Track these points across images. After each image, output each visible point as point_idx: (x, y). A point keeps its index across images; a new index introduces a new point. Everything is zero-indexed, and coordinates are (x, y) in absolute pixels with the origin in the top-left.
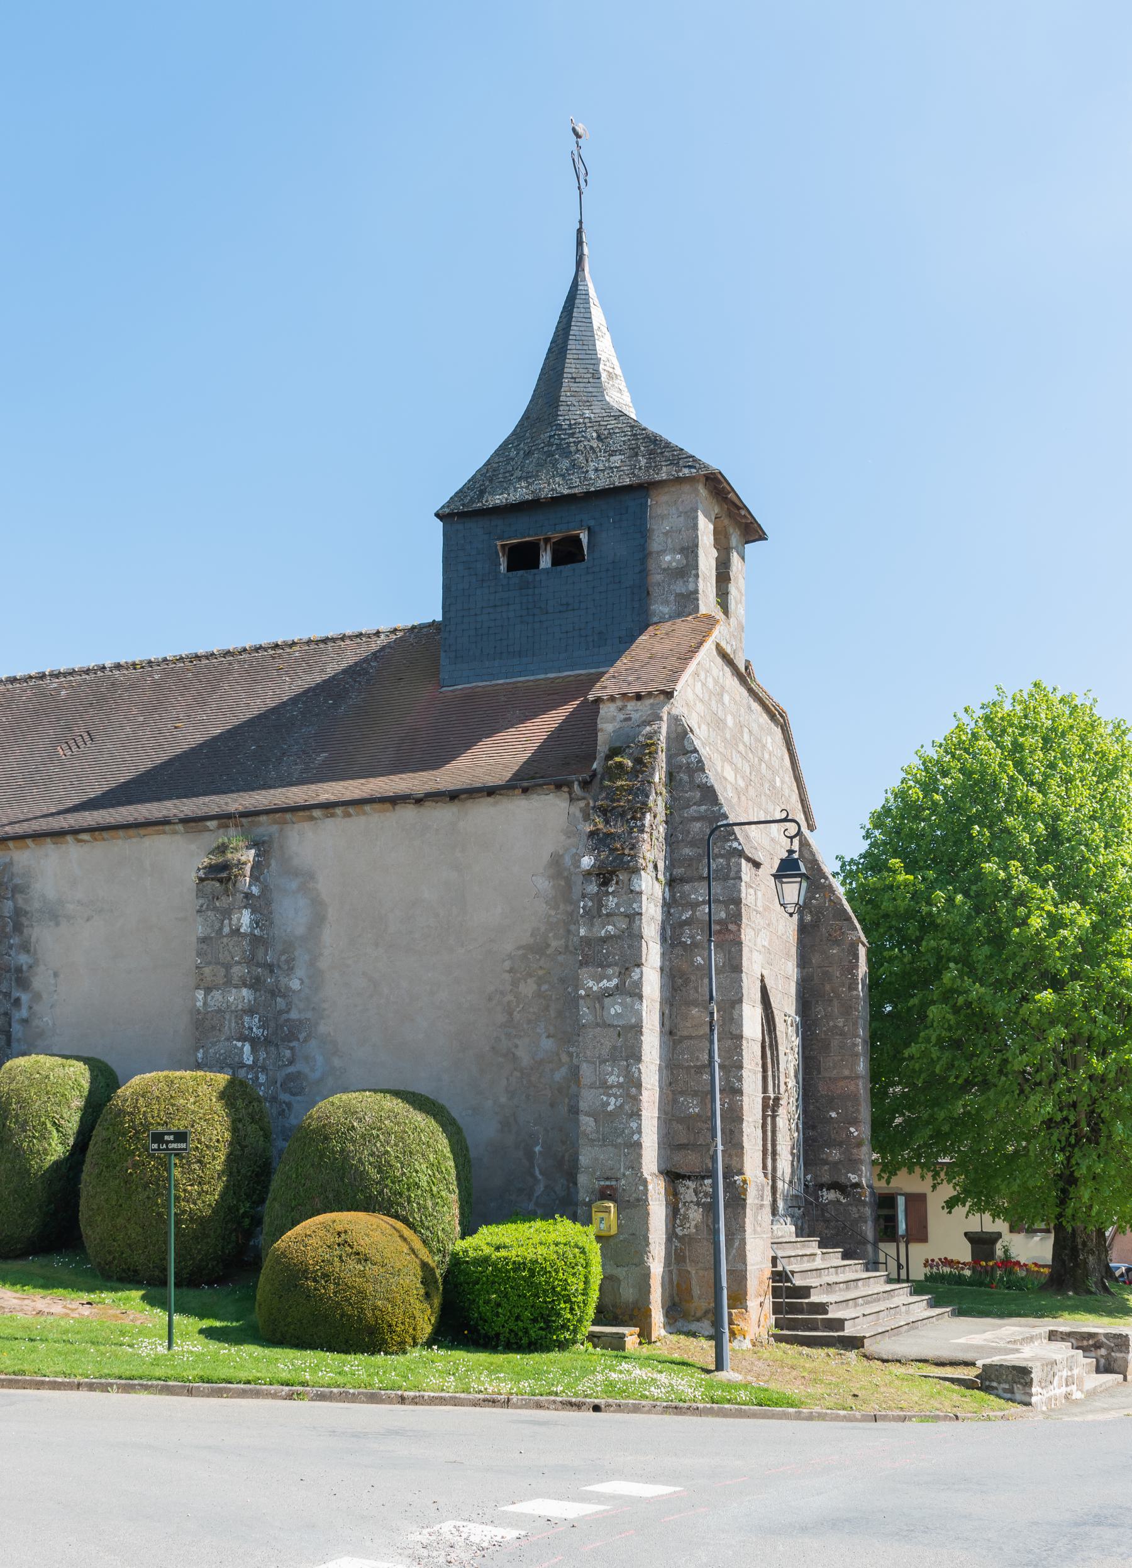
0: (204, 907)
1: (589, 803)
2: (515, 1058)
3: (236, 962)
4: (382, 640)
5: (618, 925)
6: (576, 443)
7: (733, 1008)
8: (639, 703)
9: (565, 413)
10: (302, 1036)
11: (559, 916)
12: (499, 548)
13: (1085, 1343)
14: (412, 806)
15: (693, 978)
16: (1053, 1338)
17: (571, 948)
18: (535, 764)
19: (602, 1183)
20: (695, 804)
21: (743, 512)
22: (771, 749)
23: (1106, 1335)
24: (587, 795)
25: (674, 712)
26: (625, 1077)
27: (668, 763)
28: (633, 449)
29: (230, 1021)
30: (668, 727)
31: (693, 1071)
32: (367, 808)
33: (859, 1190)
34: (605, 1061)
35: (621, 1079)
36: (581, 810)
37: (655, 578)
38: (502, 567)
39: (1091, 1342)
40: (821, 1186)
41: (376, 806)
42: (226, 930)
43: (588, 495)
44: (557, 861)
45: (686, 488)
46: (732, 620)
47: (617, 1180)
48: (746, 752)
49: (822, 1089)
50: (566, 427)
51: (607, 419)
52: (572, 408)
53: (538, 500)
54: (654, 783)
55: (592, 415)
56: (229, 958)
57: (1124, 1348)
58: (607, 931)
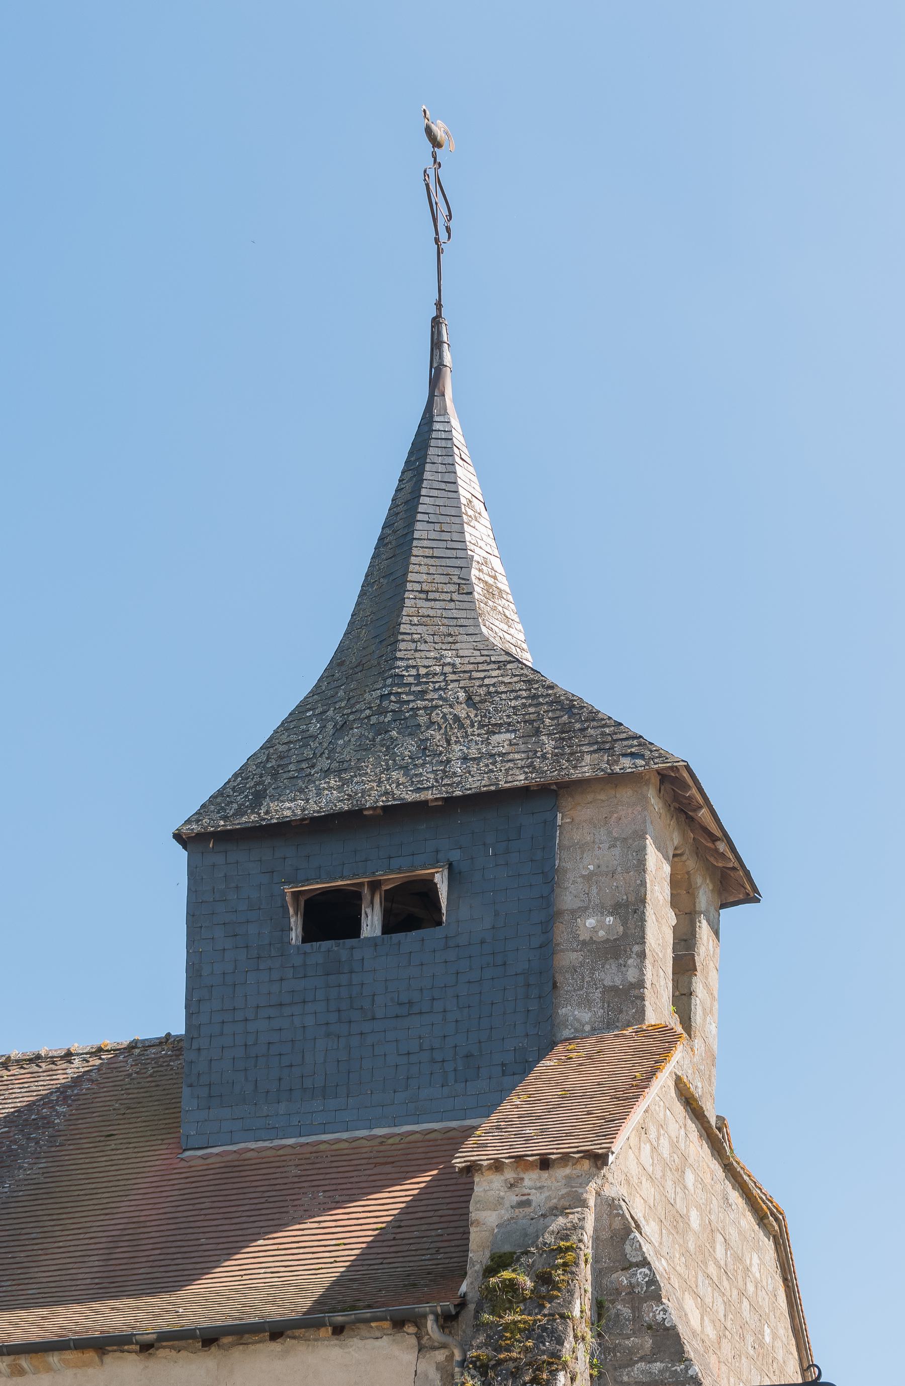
1: (453, 1355)
4: (77, 1067)
6: (429, 710)
8: (545, 1174)
9: (409, 655)
14: (133, 1356)
18: (355, 1286)
20: (642, 1359)
21: (722, 847)
22: (758, 1275)
24: (448, 1339)
25: (609, 1191)
27: (597, 1283)
28: (531, 722)
30: (597, 1220)
32: (54, 1359)
36: (439, 1367)
37: (569, 958)
38: (293, 935)
41: (69, 1355)
43: (451, 804)
45: (626, 794)
46: (698, 1043)
48: (720, 1278)
50: (411, 680)
51: (485, 667)
52: (422, 647)
53: (361, 811)
54: (572, 1319)
55: (458, 661)
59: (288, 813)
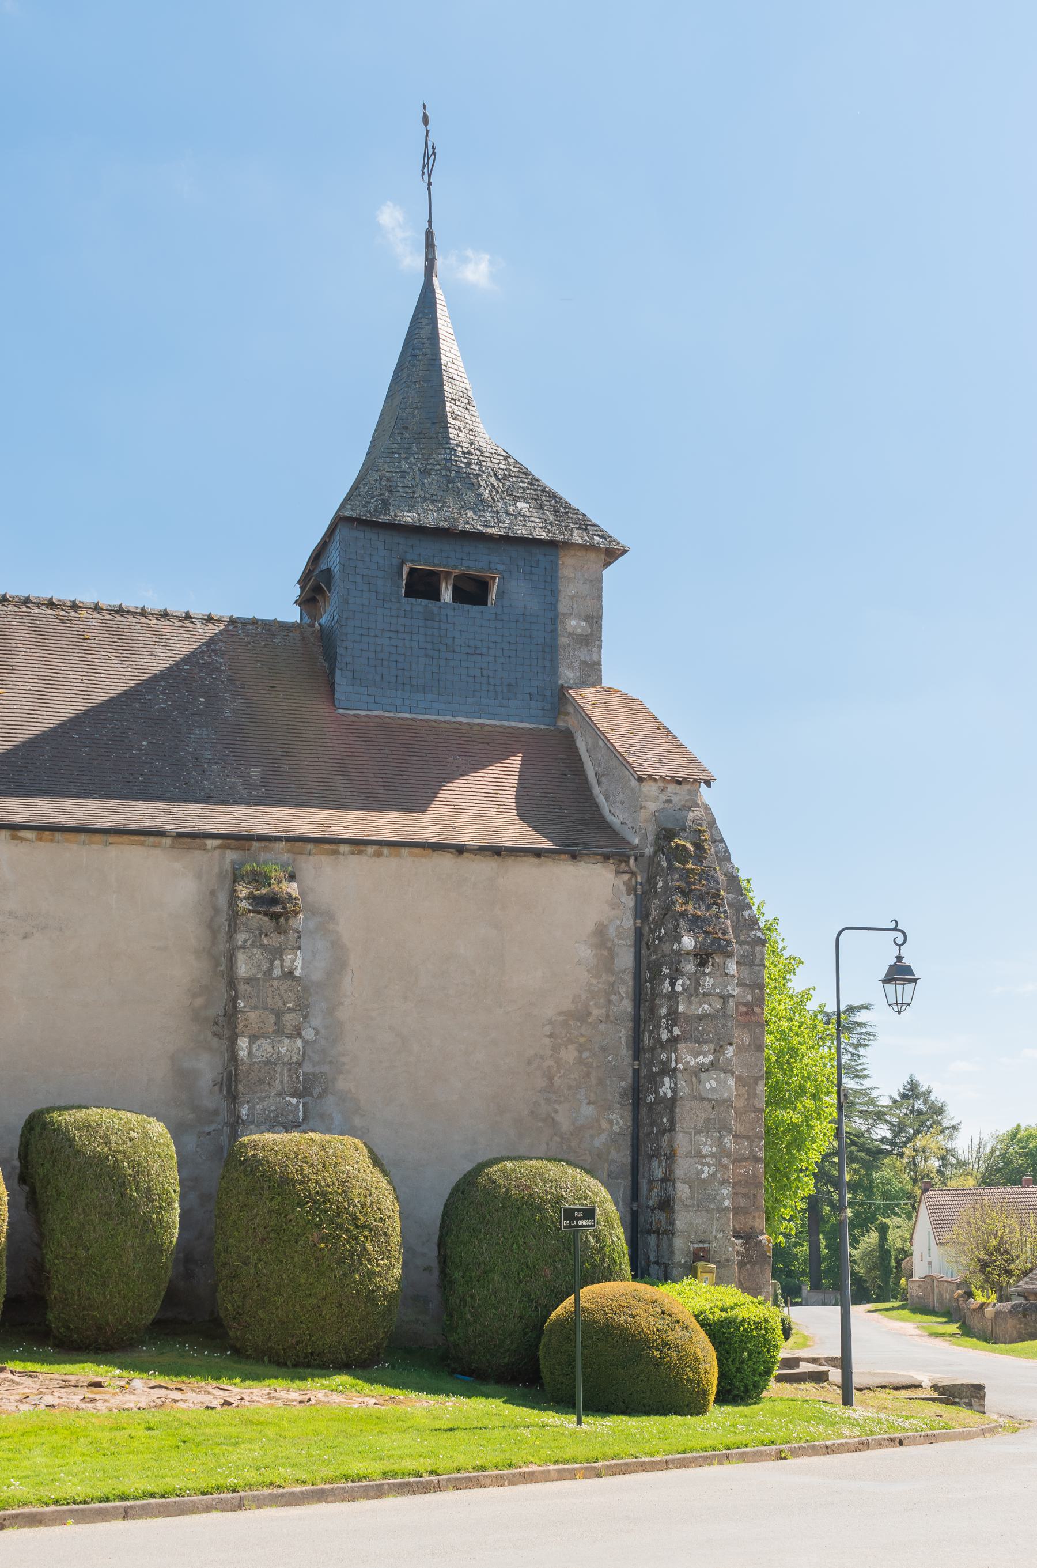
0: (249, 943)
2: (554, 1123)
3: (289, 1009)
5: (714, 1005)
11: (600, 985)
17: (612, 1018)
19: (696, 1246)
26: (718, 1147)
29: (282, 1075)
32: (405, 851)
34: (699, 1132)
35: (714, 1150)
36: (625, 883)
37: (563, 640)
41: (415, 850)
42: (277, 972)
44: (601, 931)
47: (710, 1242)
56: (280, 1004)
58: (703, 1009)
59: (409, 519)
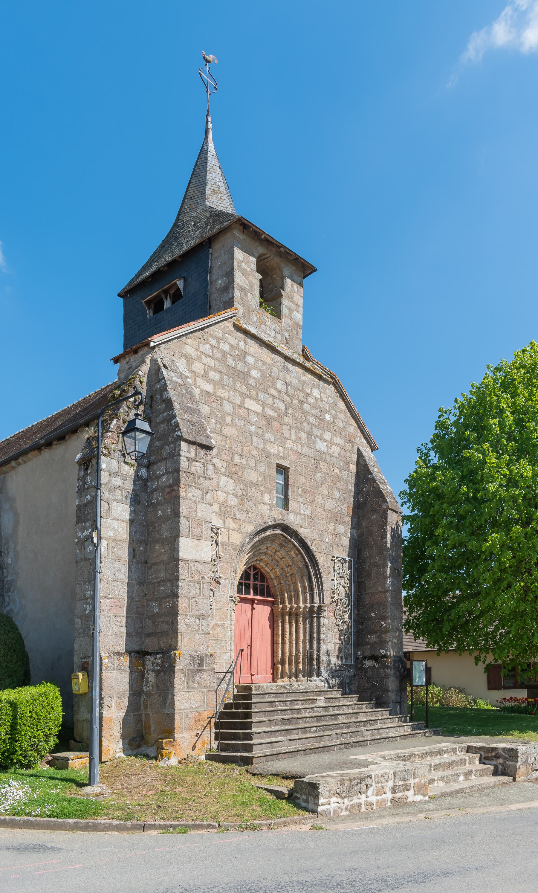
7: (175, 541)
10: (12, 589)
12: (144, 304)
13: (490, 755)
15: (157, 525)
16: (470, 751)
19: (83, 660)
23: (504, 749)
31: (156, 585)
33: (385, 659)
34: (84, 583)
39: (493, 754)
40: (365, 658)
49: (367, 600)
57: (514, 759)
